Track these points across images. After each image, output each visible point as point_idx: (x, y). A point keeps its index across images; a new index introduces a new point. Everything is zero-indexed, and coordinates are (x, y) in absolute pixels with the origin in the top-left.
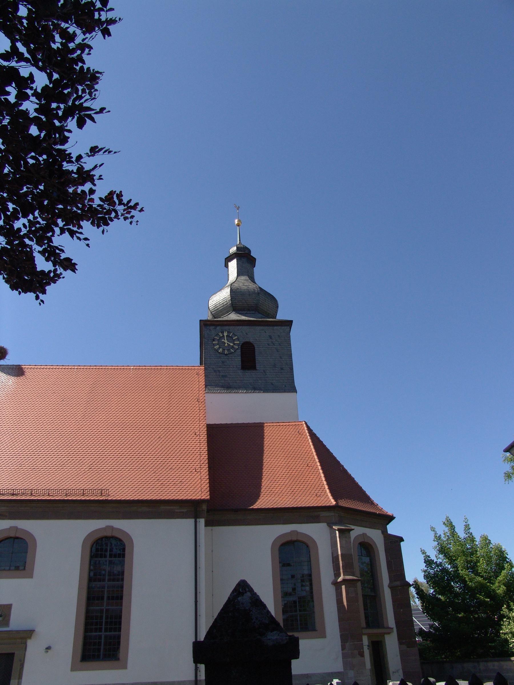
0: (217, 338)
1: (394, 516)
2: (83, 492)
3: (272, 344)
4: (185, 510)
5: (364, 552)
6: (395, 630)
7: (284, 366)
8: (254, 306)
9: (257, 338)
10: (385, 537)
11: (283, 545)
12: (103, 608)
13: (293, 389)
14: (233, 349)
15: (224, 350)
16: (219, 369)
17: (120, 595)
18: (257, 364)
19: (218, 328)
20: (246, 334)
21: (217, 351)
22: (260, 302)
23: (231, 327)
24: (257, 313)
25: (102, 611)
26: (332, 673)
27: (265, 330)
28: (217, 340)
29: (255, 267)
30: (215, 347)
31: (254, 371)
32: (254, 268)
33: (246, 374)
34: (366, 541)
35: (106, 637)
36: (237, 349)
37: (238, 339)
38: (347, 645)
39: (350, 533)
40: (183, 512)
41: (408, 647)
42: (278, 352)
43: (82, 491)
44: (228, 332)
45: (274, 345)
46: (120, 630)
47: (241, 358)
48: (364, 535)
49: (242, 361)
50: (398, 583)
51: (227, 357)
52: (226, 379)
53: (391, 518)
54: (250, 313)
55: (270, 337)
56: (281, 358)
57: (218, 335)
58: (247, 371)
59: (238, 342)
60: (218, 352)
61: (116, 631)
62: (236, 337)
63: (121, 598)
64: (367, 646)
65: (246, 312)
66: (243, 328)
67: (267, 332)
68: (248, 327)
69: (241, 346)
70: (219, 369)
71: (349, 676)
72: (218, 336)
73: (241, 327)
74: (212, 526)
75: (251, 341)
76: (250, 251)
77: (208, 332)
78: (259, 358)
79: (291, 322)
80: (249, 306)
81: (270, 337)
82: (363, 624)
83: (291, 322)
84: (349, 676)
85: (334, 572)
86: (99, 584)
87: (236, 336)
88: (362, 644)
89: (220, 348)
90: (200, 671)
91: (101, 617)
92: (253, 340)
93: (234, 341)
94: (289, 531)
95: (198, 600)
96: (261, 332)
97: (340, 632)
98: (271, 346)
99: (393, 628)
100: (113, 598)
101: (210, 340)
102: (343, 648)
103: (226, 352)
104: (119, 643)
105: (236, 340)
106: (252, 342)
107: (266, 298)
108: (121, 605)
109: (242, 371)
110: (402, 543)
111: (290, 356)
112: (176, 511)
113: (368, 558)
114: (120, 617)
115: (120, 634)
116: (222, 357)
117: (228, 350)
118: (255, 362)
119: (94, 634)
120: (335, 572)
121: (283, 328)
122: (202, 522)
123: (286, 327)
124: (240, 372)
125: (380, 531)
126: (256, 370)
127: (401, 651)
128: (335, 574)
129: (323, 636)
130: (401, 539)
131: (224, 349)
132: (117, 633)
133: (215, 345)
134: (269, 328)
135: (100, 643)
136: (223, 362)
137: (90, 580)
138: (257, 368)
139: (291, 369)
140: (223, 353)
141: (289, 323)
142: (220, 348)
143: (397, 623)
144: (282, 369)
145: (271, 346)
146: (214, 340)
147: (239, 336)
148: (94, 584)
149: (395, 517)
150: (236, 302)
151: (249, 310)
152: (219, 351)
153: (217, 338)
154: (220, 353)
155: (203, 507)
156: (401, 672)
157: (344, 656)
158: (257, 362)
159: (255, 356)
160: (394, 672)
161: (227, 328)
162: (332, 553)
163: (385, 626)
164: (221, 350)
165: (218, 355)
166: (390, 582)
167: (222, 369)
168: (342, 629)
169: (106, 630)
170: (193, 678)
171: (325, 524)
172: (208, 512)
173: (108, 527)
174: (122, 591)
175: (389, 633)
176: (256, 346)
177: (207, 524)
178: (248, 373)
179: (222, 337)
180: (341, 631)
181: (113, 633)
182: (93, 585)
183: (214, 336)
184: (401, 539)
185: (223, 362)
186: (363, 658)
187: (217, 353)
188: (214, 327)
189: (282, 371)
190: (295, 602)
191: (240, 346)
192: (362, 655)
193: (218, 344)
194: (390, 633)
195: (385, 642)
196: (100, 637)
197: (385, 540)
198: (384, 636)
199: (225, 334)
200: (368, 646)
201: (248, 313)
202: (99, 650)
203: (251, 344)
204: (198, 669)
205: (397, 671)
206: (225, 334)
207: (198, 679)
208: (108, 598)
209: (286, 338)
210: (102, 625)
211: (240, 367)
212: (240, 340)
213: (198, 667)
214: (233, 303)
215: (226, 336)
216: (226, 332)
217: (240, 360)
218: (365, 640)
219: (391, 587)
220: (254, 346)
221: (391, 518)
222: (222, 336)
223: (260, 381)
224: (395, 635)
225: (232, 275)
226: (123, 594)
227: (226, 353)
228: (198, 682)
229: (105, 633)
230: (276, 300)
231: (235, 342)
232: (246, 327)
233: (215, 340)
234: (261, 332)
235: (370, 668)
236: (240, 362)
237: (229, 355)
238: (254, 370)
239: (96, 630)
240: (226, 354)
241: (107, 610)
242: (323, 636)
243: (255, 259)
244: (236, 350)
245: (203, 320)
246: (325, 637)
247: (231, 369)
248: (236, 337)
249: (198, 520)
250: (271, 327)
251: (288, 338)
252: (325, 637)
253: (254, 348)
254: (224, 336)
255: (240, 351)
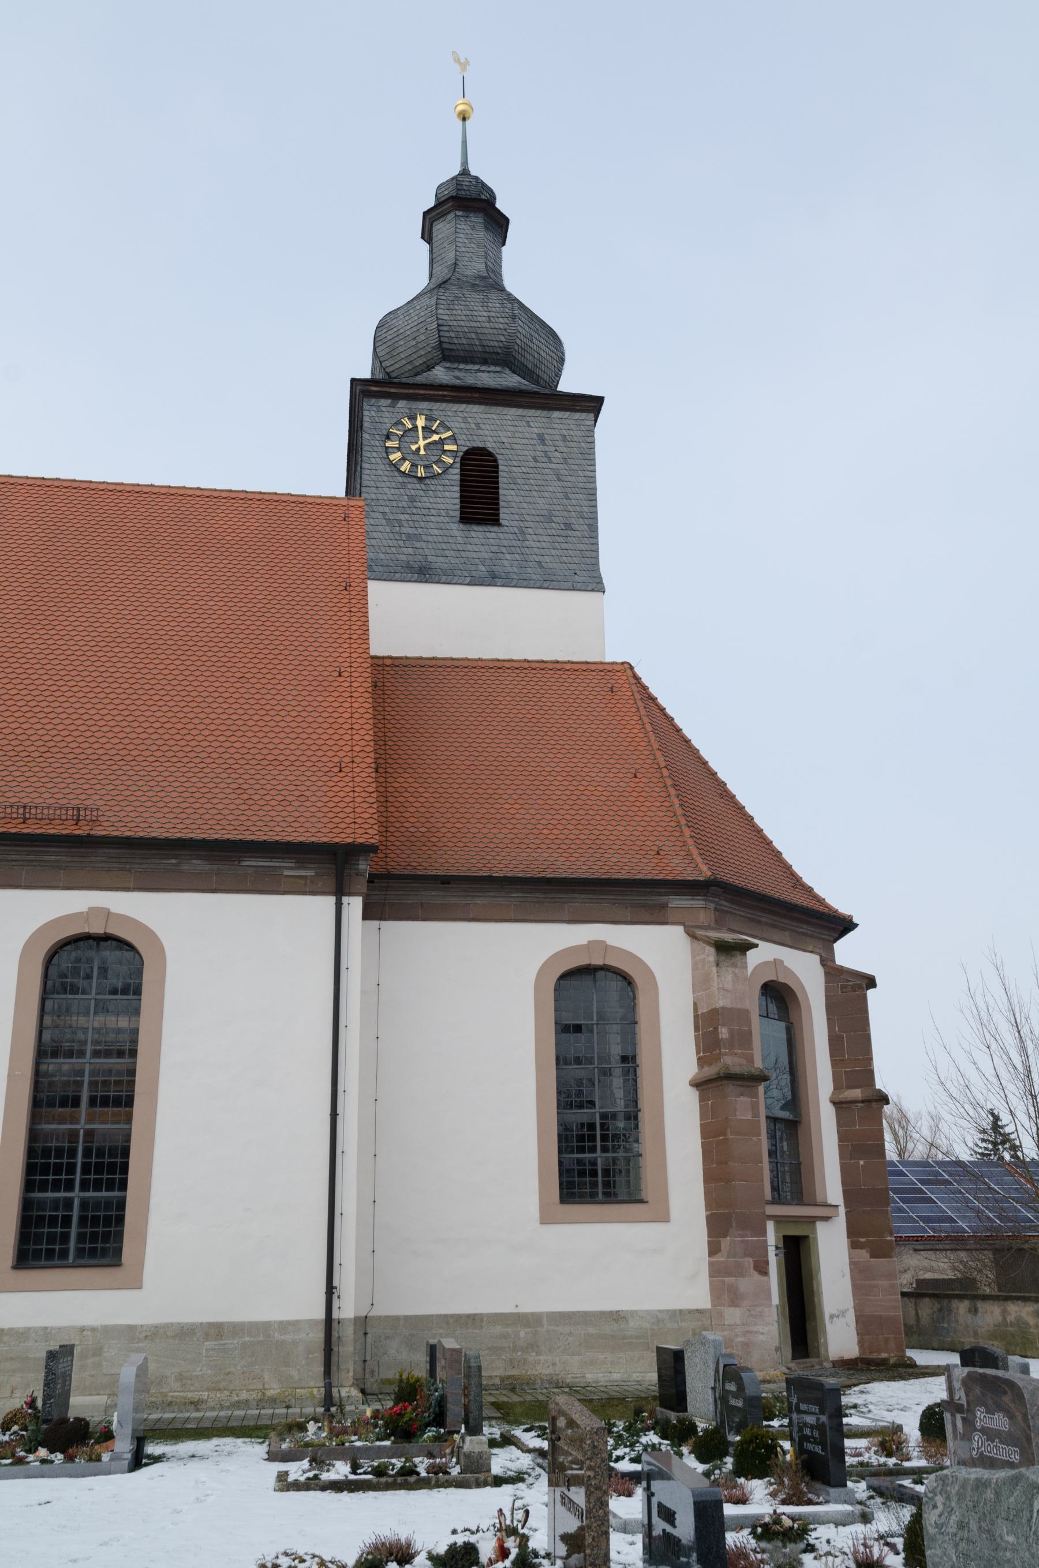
0: (398, 432)
1: (855, 920)
2: (24, 814)
3: (546, 459)
4: (311, 873)
5: (773, 1008)
6: (842, 1210)
7: (573, 521)
8: (499, 351)
9: (504, 440)
10: (827, 974)
11: (566, 976)
12: (78, 1127)
13: (595, 584)
14: (440, 465)
15: (414, 465)
16: (402, 517)
17: (124, 1094)
18: (502, 510)
19: (402, 404)
20: (477, 425)
21: (395, 466)
22: (518, 342)
23: (436, 406)
24: (507, 371)
25: (73, 1135)
26: (681, 1311)
27: (528, 419)
28: (397, 438)
29: (504, 244)
30: (392, 457)
31: (495, 529)
32: (504, 249)
33: (473, 534)
34: (782, 980)
35: (84, 1204)
36: (451, 466)
37: (454, 439)
38: (725, 1243)
39: (745, 955)
40: (306, 877)
41: (873, 1256)
42: (559, 480)
43: (21, 811)
44: (430, 419)
45: (551, 462)
46: (123, 1185)
47: (461, 491)
48: (777, 963)
49: (464, 500)
50: (856, 1093)
51: (423, 487)
52: (418, 545)
53: (845, 926)
54: (489, 372)
55: (542, 439)
56: (568, 498)
57: (399, 423)
58: (475, 527)
59: (454, 448)
60: (399, 470)
61: (113, 1190)
62: (449, 433)
63: (129, 1102)
64: (774, 1248)
65: (477, 367)
66: (468, 410)
67: (531, 424)
68: (482, 408)
69: (462, 459)
70: (402, 517)
71: (726, 1323)
72: (400, 427)
73: (463, 407)
74: (381, 919)
75: (490, 445)
76: (493, 196)
77: (373, 413)
78: (507, 494)
79: (599, 401)
80: (487, 349)
81: (542, 439)
82: (768, 1194)
83: (599, 401)
84: (726, 1323)
85: (698, 1053)
86: (66, 1064)
87: (448, 429)
88: (766, 1241)
89: (404, 459)
90: (339, 1297)
91: (72, 1152)
92: (494, 445)
93: (443, 444)
94: (585, 942)
95: (340, 1110)
96: (516, 423)
97: (706, 1206)
98: (543, 465)
99: (837, 1206)
100: (105, 1102)
101: (377, 437)
102: (714, 1249)
103: (421, 472)
104: (121, 1220)
105: (448, 441)
106: (490, 450)
107: (533, 333)
108: (129, 1120)
109: (461, 526)
110: (871, 993)
111: (591, 494)
112: (286, 873)
113: (783, 1024)
114: (126, 1152)
115: (125, 1197)
116: (409, 486)
117: (426, 467)
118: (498, 504)
119: (50, 1195)
120: (702, 1054)
121: (577, 415)
122: (354, 905)
123: (584, 415)
124: (456, 529)
125: (817, 958)
126: (499, 525)
127: (854, 1265)
128: (699, 1059)
129: (663, 1217)
130: (871, 982)
131: (416, 462)
132: (116, 1193)
133: (390, 450)
134: (538, 413)
135: (67, 1221)
136: (412, 499)
137: (42, 1052)
138: (501, 521)
139: (593, 529)
140: (411, 475)
141: (592, 405)
142: (404, 459)
143: (847, 1194)
144: (568, 527)
145: (543, 465)
146: (388, 437)
147: (456, 431)
148: (51, 1065)
149: (857, 925)
150: (453, 335)
151: (485, 362)
152: (402, 469)
153: (398, 432)
154: (404, 473)
155: (361, 867)
156: (851, 1316)
157: (716, 1271)
158: (501, 504)
159: (498, 488)
160: (832, 1317)
161: (424, 405)
162: (695, 1004)
163: (819, 1199)
164: (406, 467)
165: (400, 479)
166: (835, 1088)
167: (407, 517)
168: (712, 1200)
169: (84, 1187)
170: (319, 1313)
171: (680, 929)
172: (372, 882)
173: (93, 911)
174: (132, 1083)
175: (826, 1219)
176: (500, 462)
177: (368, 914)
178: (478, 533)
179: (410, 430)
180: (708, 1206)
181: (104, 1194)
182: (51, 1067)
183: (388, 426)
184: (871, 982)
185: (412, 499)
186: (766, 1278)
187: (396, 474)
188: (389, 401)
189: (570, 533)
190: (592, 1126)
191: (458, 460)
192: (762, 1269)
193: (399, 449)
194: (831, 1217)
195: (815, 1239)
196: (68, 1203)
197: (826, 983)
198: (814, 1222)
199: (421, 422)
200: (777, 1248)
201: (483, 371)
202: (65, 1238)
203: (490, 454)
204: (334, 1290)
205: (843, 1313)
206: (421, 422)
207: (335, 1315)
208: (92, 1102)
209: (583, 444)
210: (74, 1173)
211: (458, 513)
212: (459, 443)
213: (334, 1285)
214: (443, 339)
215: (423, 428)
216: (423, 417)
217: (458, 495)
218: (772, 1237)
219: (837, 1103)
220: (496, 460)
221: (845, 926)
222: (410, 426)
223: (508, 556)
224: (840, 1223)
225: (441, 262)
226: (134, 1091)
227: (419, 475)
228: (335, 1325)
229: (82, 1194)
230: (560, 342)
231: (446, 447)
232: (477, 406)
233: (391, 437)
234: (516, 423)
235: (778, 1303)
236: (458, 501)
237: (427, 481)
238: (493, 525)
239: (56, 1186)
240: (421, 479)
241: (89, 1134)
242: (663, 1217)
243: (507, 220)
244: (448, 469)
245: (360, 380)
246: (668, 1221)
247: (433, 519)
248: (449, 433)
249: (345, 900)
250: (545, 413)
251: (589, 446)
252: (668, 1221)
253: (497, 467)
254: (415, 427)
255: (458, 471)
